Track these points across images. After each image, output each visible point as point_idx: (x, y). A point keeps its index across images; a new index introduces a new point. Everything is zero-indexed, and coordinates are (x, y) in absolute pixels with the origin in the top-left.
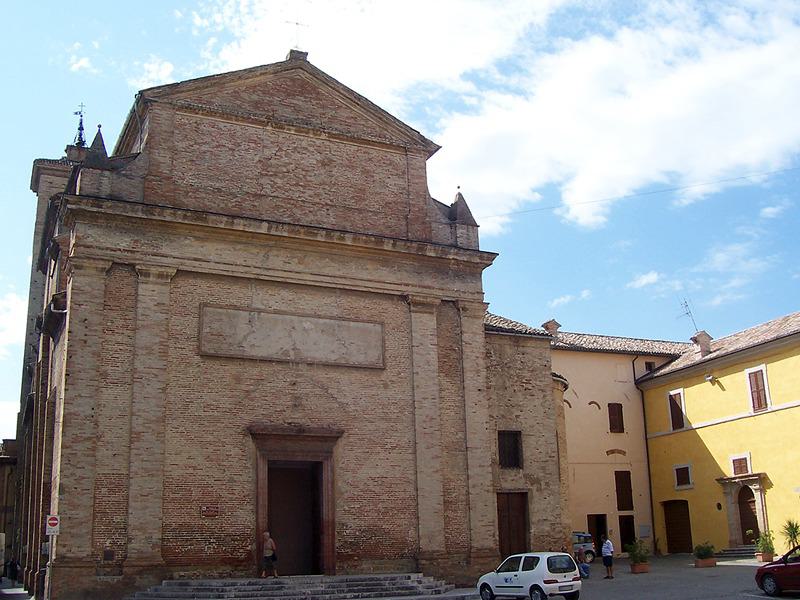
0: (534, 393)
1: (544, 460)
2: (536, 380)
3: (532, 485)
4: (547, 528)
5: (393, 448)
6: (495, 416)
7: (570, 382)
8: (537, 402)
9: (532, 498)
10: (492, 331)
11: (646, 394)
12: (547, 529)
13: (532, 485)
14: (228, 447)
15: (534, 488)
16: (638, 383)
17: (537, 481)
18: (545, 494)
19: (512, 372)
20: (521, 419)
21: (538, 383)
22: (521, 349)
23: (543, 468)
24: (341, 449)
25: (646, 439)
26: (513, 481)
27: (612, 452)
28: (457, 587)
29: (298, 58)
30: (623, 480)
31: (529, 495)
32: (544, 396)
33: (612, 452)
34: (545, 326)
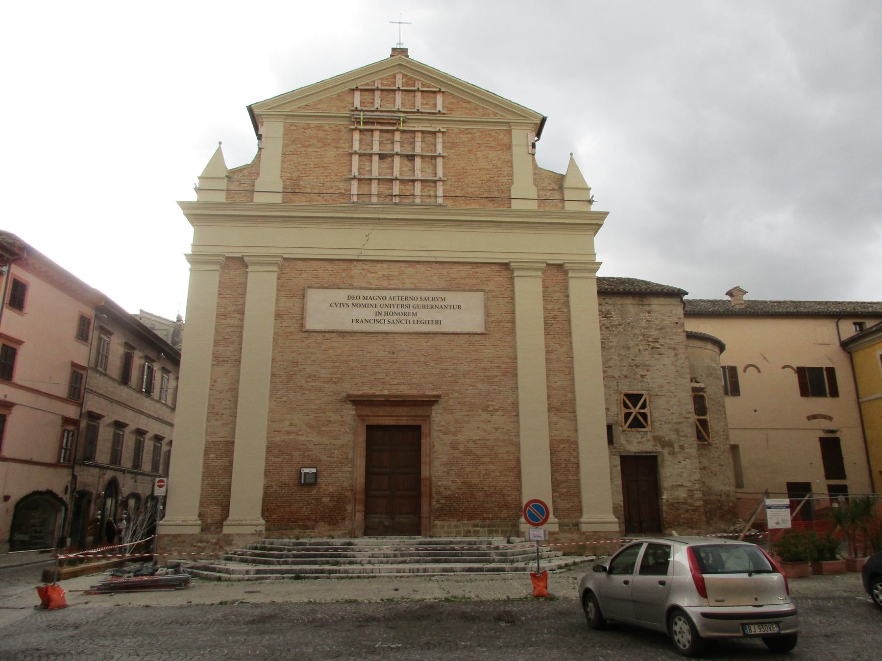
0: (663, 351)
1: (678, 421)
2: (665, 338)
3: (663, 448)
4: (682, 494)
5: (497, 410)
6: (616, 376)
7: (723, 340)
8: (667, 361)
9: (663, 461)
10: (613, 290)
11: (855, 355)
12: (685, 495)
13: (663, 448)
14: (328, 414)
15: (666, 451)
16: (845, 345)
17: (670, 444)
18: (680, 457)
19: (636, 331)
20: (648, 379)
21: (668, 341)
22: (646, 308)
23: (677, 431)
24: (438, 415)
25: (859, 404)
26: (636, 443)
27: (815, 417)
28: (564, 555)
29: (400, 52)
30: (831, 448)
31: (659, 459)
32: (676, 355)
33: (815, 417)
34: (729, 293)
